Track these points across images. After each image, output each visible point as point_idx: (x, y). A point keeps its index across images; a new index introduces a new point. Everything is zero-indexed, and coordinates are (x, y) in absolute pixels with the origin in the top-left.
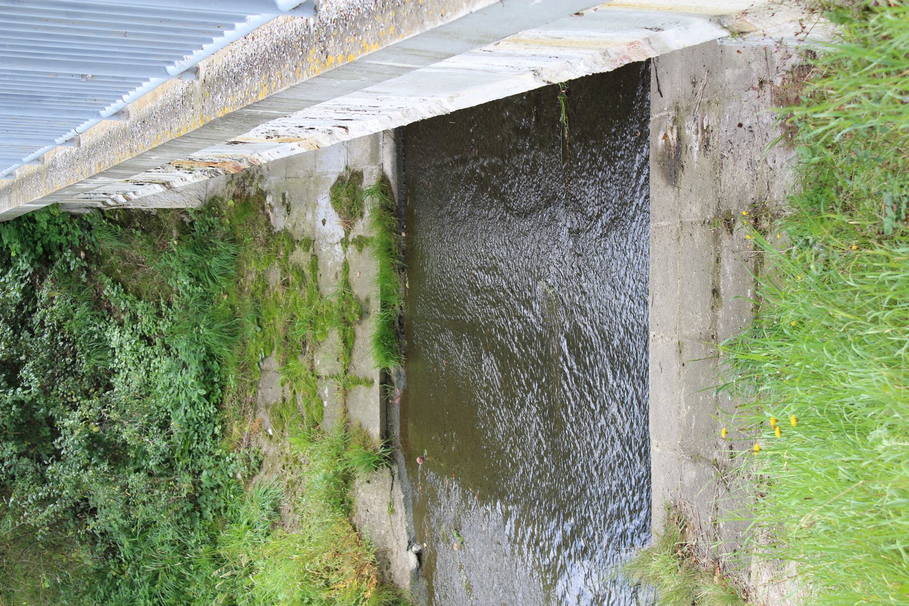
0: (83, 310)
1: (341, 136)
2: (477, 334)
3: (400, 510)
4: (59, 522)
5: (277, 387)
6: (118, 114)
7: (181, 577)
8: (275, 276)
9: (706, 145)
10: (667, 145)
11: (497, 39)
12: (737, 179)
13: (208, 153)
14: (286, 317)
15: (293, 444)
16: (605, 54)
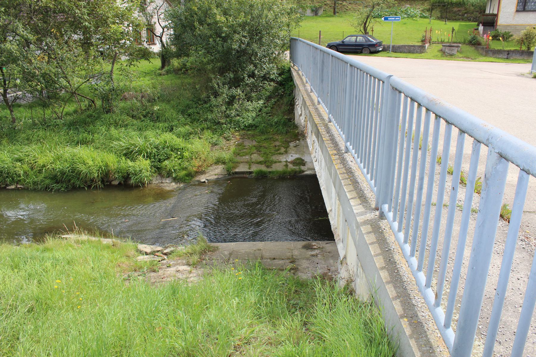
0: (268, 94)
1: (314, 160)
2: (263, 196)
3: (216, 177)
4: (213, 89)
5: (248, 144)
6: (319, 102)
7: (199, 120)
8: (277, 143)
9: (313, 256)
10: (313, 246)
11: (339, 200)
12: (304, 264)
13: (309, 125)
14: (267, 146)
15: (233, 148)
16: (336, 228)
